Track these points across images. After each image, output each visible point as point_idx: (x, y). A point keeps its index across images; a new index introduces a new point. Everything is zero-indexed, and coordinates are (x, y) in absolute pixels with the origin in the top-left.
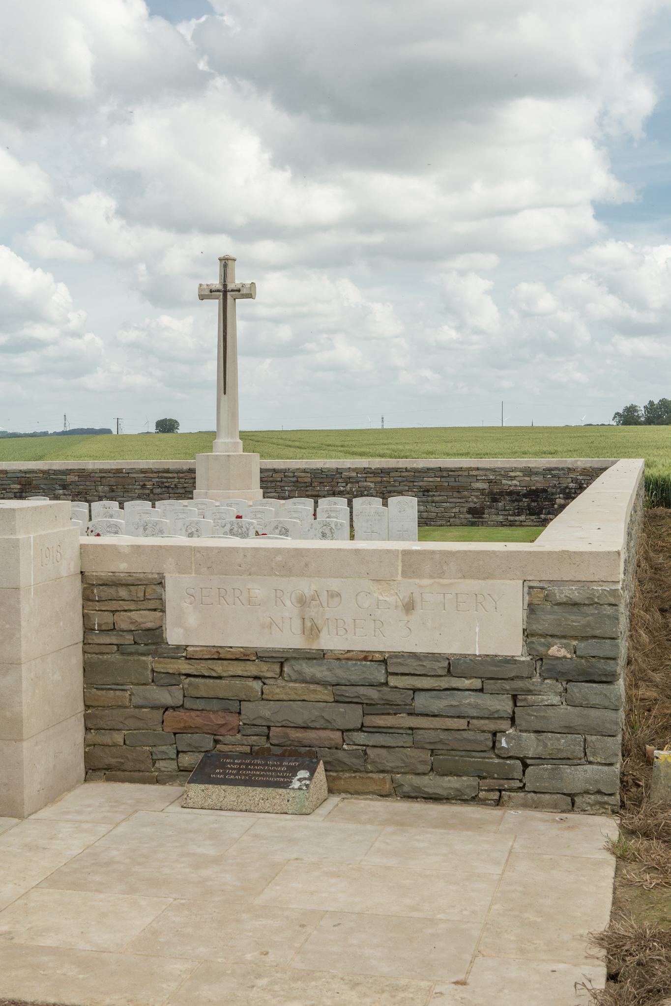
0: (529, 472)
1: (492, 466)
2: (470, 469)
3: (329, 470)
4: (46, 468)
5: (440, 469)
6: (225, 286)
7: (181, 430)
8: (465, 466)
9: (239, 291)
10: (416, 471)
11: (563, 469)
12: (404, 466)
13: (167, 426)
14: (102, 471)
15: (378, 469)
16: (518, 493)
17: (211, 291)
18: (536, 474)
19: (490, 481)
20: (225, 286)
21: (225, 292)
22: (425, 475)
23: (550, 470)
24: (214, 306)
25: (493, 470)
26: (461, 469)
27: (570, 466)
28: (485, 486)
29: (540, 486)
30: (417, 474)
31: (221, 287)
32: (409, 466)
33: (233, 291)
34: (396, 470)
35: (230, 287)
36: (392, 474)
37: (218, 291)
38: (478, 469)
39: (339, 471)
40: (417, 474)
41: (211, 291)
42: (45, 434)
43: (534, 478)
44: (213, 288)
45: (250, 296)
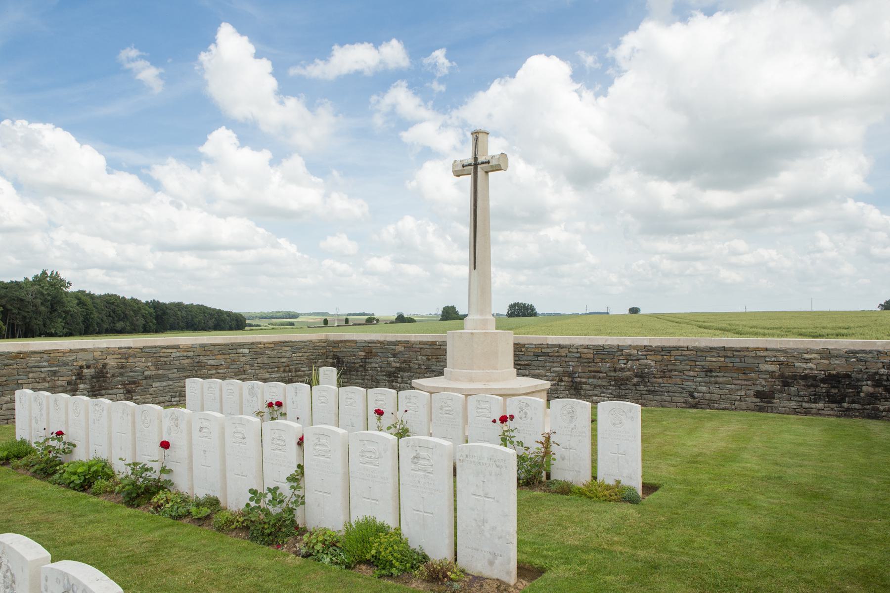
0: (827, 354)
1: (783, 347)
2: (757, 349)
3: (611, 347)
4: (382, 339)
5: (724, 349)
6: (476, 158)
7: (642, 312)
8: (751, 345)
9: (488, 162)
10: (698, 350)
11: (870, 352)
12: (686, 345)
13: (634, 311)
14: (421, 343)
15: (658, 347)
16: (814, 378)
17: (463, 166)
18: (837, 356)
19: (781, 364)
20: (476, 158)
21: (476, 165)
22: (707, 354)
23: (854, 352)
24: (468, 179)
25: (784, 351)
26: (747, 349)
27: (880, 349)
28: (775, 368)
29: (842, 371)
30: (699, 353)
31: (472, 161)
32: (691, 345)
33: (482, 163)
34: (677, 348)
35: (479, 161)
36: (673, 353)
37: (469, 165)
38: (766, 349)
39: (620, 348)
40: (699, 353)
41: (463, 166)
42: (559, 314)
43: (835, 361)
44: (466, 163)
45: (498, 168)
